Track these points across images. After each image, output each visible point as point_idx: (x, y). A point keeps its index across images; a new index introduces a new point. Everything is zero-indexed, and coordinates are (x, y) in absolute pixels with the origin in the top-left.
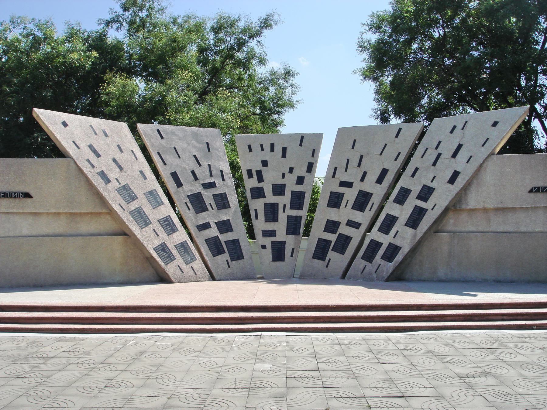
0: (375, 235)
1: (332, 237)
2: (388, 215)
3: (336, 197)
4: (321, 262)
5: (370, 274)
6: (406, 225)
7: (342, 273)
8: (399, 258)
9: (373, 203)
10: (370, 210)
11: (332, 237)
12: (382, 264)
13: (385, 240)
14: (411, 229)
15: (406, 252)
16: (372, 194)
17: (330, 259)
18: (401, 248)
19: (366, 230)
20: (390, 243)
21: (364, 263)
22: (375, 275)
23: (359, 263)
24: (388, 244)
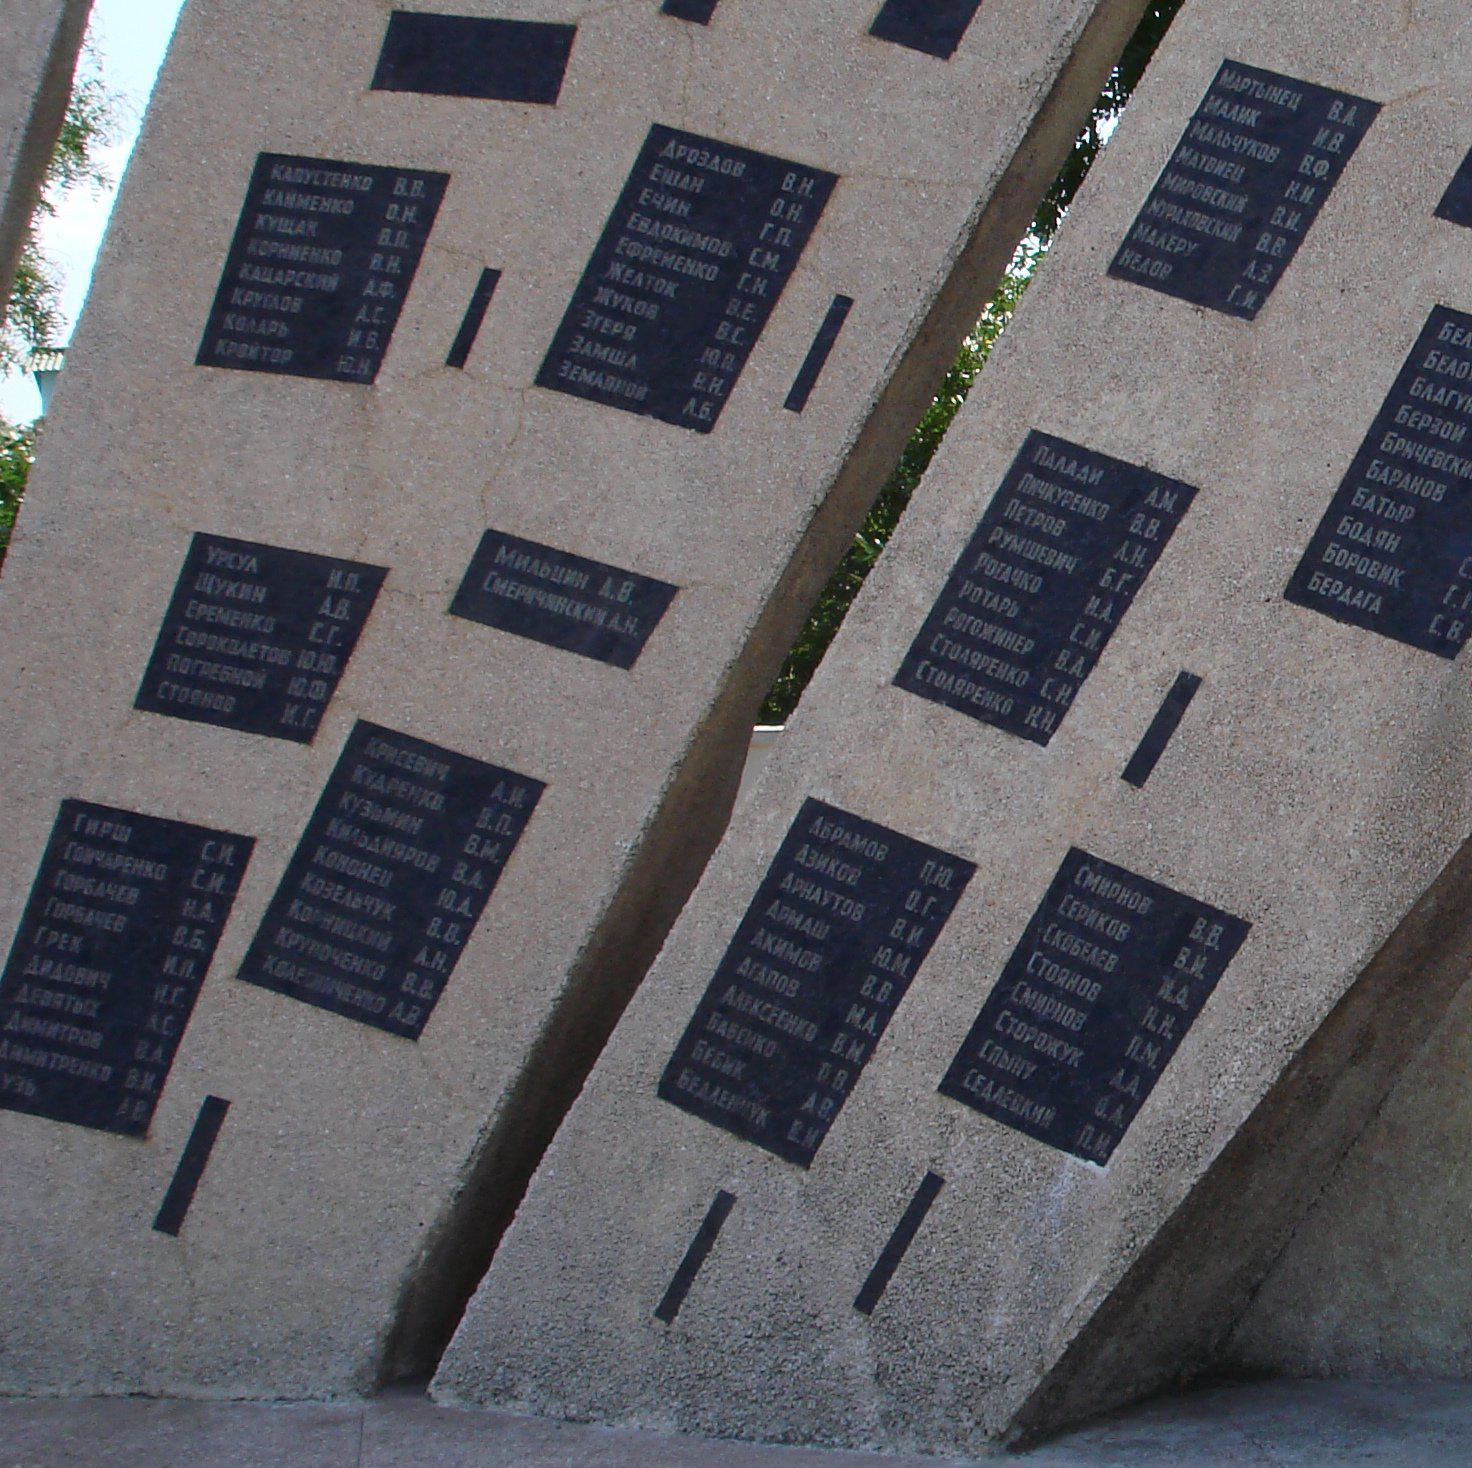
0: (867, 743)
1: (258, 790)
2: (1041, 457)
3: (332, 230)
4: (84, 1151)
5: (794, 1325)
6: (1299, 590)
7: (384, 1314)
8: (1214, 1076)
9: (841, 307)
10: (797, 399)
11: (258, 790)
12: (958, 1171)
13: (1006, 811)
14: (1384, 653)
15: (1316, 1000)
16: (825, 183)
17: (214, 1110)
18: (1236, 930)
19: (1005, 188)
20: (1076, 858)
21: (701, 1154)
22: (855, 1346)
23: (637, 1157)
24: (1048, 869)
